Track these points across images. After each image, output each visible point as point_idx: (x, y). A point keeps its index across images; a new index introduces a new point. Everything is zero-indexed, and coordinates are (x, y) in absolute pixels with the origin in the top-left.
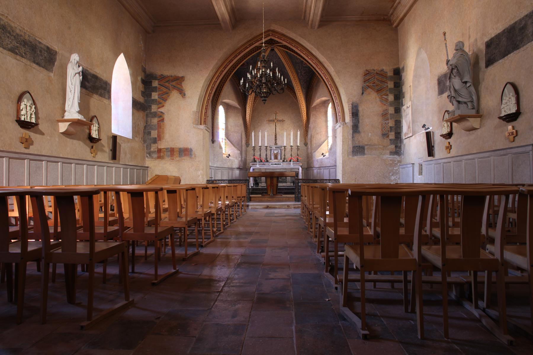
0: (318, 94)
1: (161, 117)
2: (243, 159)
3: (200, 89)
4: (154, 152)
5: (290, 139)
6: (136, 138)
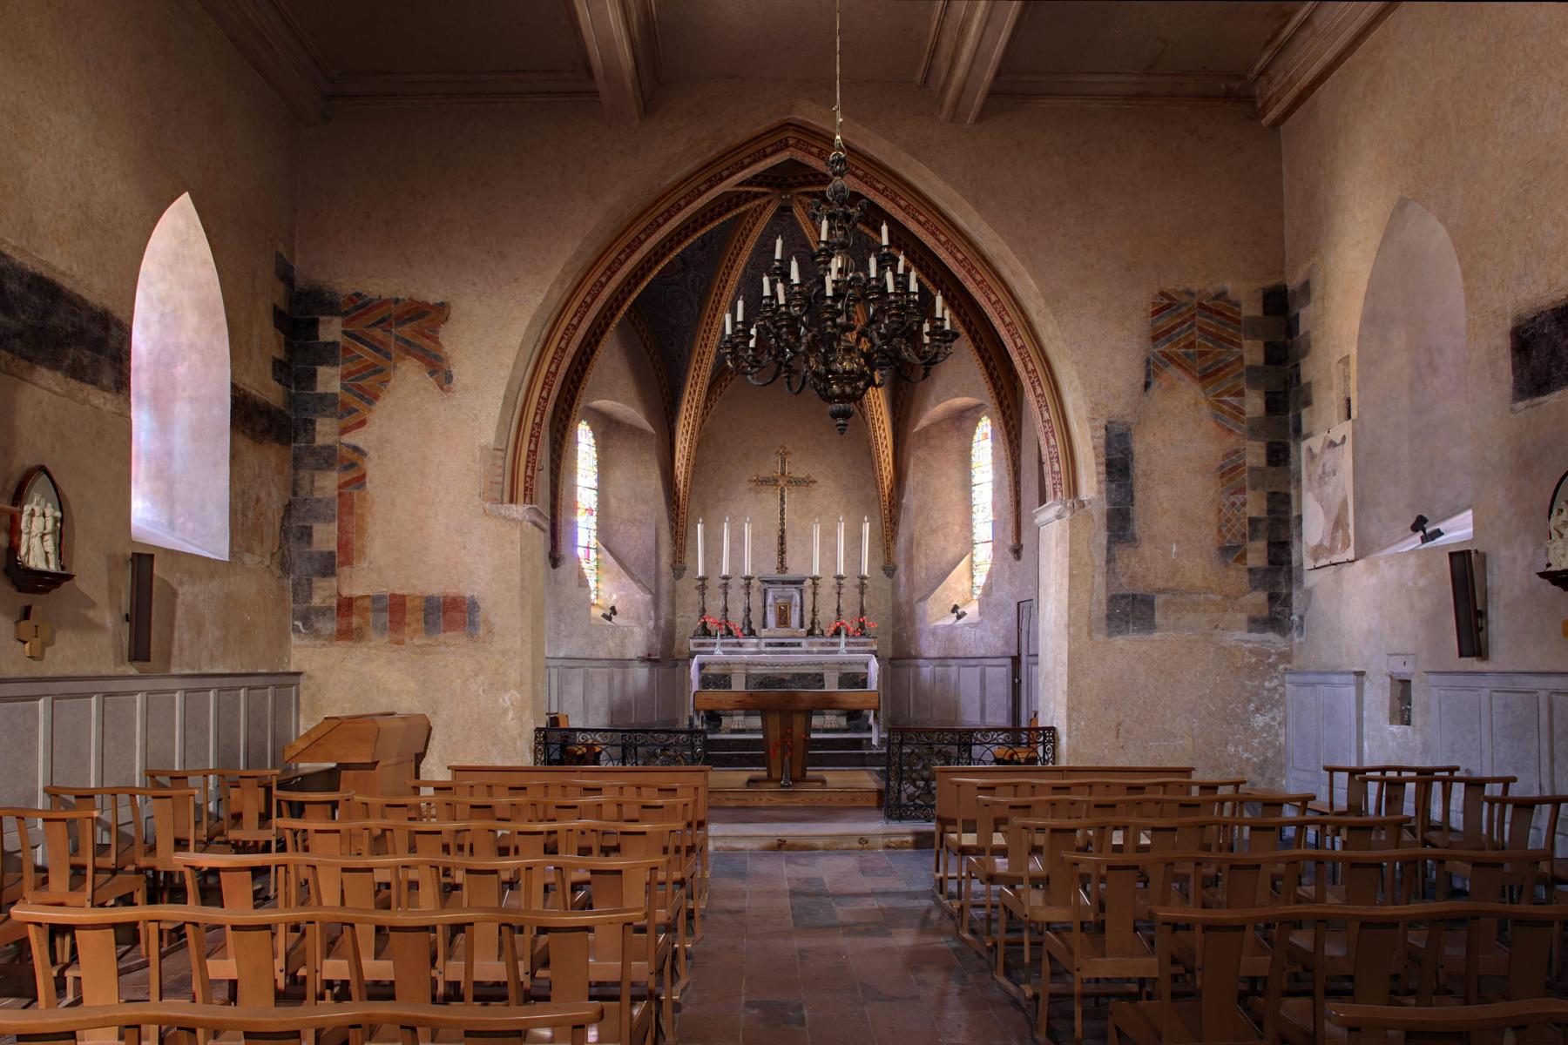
1: (352, 466)
2: (662, 623)
3: (512, 354)
4: (323, 612)
5: (835, 548)
6: (247, 558)
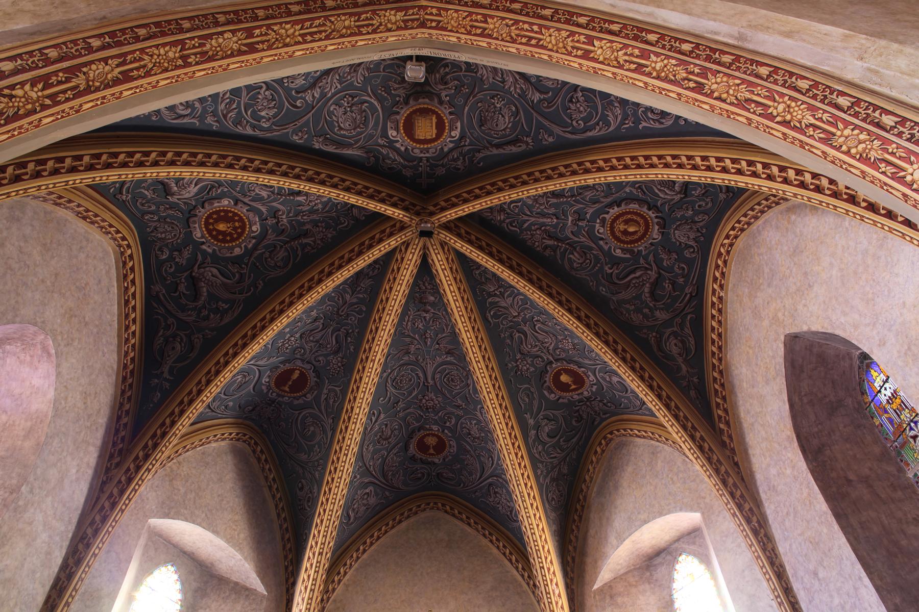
0: (618, 521)
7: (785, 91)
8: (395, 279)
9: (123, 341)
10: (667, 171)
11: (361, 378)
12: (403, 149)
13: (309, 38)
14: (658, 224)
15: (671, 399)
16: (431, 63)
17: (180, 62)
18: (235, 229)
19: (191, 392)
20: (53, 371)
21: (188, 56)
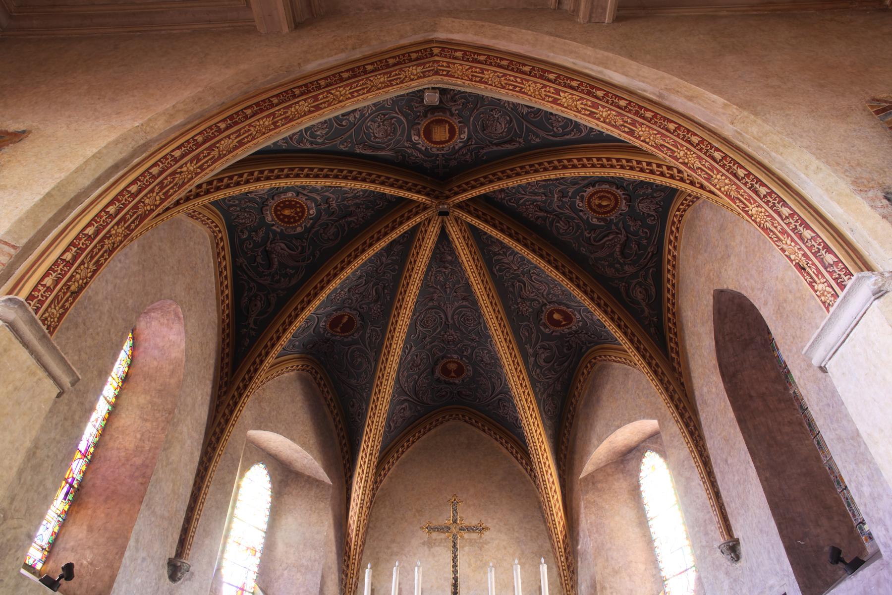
0: (599, 427)
7: (684, 143)
8: (420, 246)
9: (220, 302)
10: (622, 171)
11: (397, 322)
12: (423, 149)
13: (356, 94)
14: (625, 199)
15: (634, 335)
16: (443, 92)
17: (272, 127)
18: (297, 213)
19: (272, 338)
20: (182, 330)
21: (277, 122)
